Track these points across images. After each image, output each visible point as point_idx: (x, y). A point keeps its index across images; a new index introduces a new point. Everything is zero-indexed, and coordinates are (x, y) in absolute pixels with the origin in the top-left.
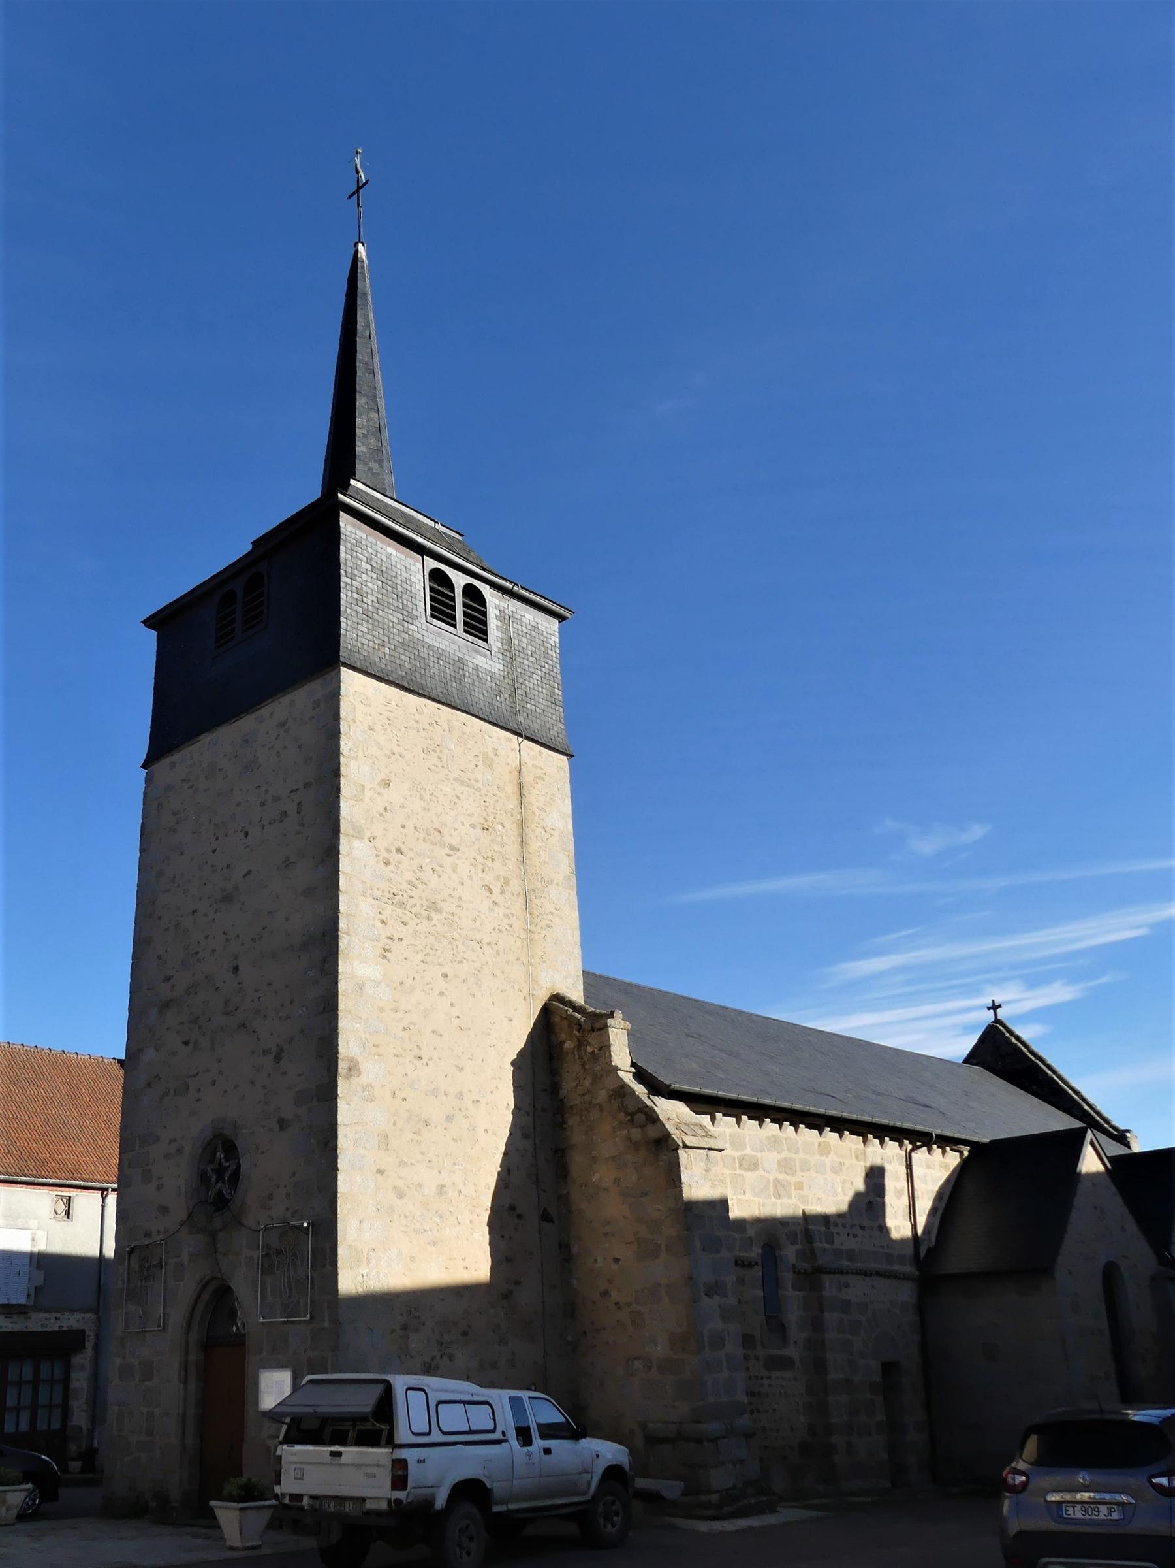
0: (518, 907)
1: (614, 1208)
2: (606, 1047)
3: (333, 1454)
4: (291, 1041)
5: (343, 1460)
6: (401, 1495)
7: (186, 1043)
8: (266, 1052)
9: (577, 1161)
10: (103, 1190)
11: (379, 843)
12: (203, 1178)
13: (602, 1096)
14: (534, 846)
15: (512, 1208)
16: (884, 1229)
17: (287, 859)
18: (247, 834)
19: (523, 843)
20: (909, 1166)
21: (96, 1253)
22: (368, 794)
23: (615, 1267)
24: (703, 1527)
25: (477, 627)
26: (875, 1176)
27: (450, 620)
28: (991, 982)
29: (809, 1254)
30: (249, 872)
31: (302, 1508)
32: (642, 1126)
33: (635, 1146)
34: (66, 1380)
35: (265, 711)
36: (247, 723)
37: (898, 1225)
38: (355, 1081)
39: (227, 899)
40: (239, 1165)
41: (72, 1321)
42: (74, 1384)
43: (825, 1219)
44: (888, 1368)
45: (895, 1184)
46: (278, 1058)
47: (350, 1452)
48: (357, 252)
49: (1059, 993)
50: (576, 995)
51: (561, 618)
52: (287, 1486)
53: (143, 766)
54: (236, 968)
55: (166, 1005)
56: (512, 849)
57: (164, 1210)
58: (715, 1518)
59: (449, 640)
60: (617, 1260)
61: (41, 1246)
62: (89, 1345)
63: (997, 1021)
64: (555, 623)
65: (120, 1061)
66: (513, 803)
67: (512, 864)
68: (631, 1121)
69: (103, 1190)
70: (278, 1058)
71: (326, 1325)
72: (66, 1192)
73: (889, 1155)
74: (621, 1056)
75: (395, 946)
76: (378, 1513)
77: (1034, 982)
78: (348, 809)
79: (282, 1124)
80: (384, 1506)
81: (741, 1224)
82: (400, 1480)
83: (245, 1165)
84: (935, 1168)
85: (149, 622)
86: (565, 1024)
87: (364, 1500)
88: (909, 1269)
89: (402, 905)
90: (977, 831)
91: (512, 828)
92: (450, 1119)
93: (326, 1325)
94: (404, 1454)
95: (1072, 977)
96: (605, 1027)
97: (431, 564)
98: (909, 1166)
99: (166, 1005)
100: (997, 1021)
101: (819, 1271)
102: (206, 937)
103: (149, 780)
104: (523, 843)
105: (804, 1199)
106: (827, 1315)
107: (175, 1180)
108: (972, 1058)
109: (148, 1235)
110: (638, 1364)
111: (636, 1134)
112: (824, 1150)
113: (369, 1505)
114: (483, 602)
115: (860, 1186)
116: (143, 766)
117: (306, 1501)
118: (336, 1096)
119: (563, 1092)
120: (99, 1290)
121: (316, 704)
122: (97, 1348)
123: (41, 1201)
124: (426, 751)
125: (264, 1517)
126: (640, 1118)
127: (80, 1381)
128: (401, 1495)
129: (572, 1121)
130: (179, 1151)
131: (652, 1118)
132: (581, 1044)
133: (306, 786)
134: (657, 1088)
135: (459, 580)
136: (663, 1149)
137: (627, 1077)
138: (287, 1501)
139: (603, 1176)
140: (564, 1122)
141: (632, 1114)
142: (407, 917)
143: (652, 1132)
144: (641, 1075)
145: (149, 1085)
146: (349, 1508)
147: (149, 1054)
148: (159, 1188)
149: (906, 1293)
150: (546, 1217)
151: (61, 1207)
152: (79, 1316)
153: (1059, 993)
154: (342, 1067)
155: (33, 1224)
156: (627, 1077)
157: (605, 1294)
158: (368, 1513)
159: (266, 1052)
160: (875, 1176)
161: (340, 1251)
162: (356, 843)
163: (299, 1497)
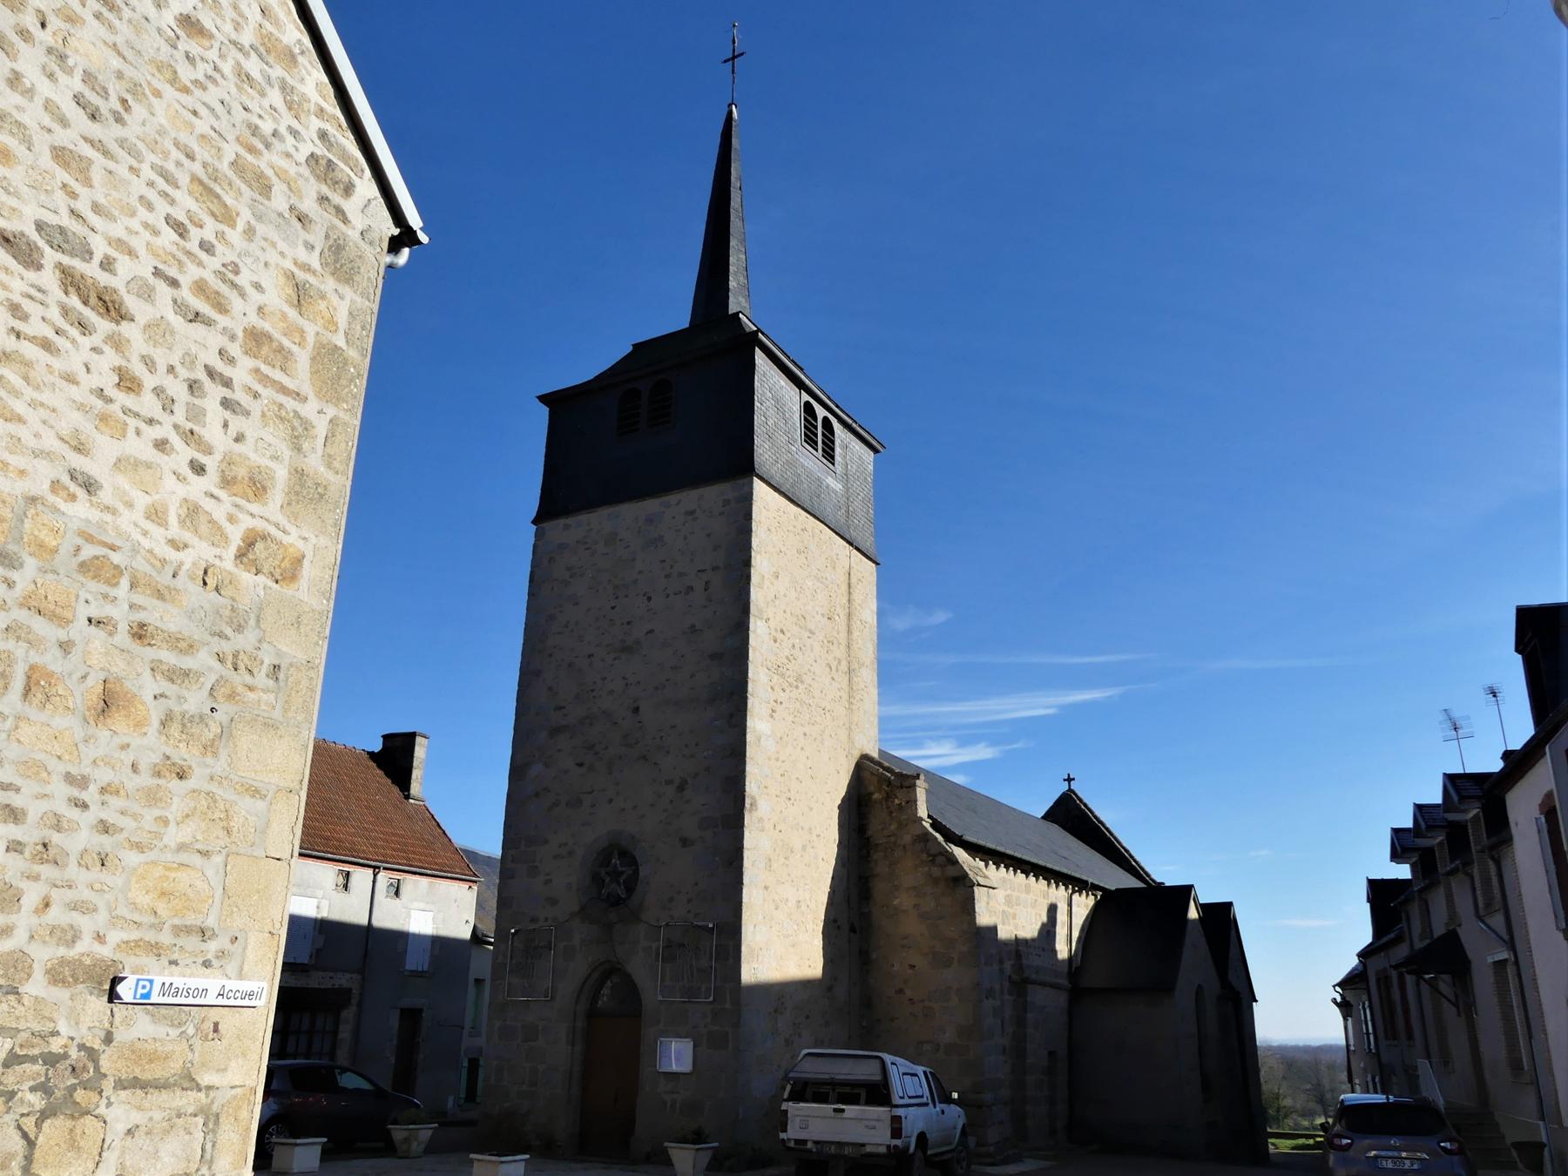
0: (845, 684)
1: (911, 926)
2: (913, 802)
3: (835, 1110)
4: (696, 775)
5: (845, 1115)
6: (898, 1142)
7: (580, 765)
8: (668, 782)
9: (879, 888)
10: (375, 868)
11: (772, 623)
12: (597, 880)
13: (907, 839)
14: (856, 634)
15: (835, 921)
16: (1054, 952)
17: (693, 626)
18: (649, 599)
19: (849, 632)
20: (1070, 905)
21: (365, 922)
22: (767, 583)
23: (910, 971)
24: (989, 1169)
25: (829, 454)
26: (1052, 909)
27: (813, 444)
28: (931, 738)
29: (1019, 967)
30: (651, 631)
31: (810, 1151)
32: (942, 866)
33: (936, 881)
34: (335, 1032)
35: (672, 498)
36: (651, 505)
37: (1062, 950)
38: (755, 814)
39: (626, 649)
40: (636, 872)
41: (342, 980)
42: (341, 1036)
43: (1025, 941)
44: (1051, 1054)
45: (1062, 917)
46: (681, 788)
47: (851, 1110)
48: (730, 112)
49: (982, 752)
50: (875, 755)
51: (876, 451)
52: (792, 1133)
53: (534, 522)
54: (636, 710)
55: (556, 731)
56: (843, 636)
57: (553, 901)
58: (993, 1164)
59: (810, 460)
60: (912, 967)
61: (324, 914)
62: (354, 1001)
63: (1070, 790)
64: (869, 456)
65: (372, 755)
66: (845, 600)
67: (843, 648)
68: (933, 861)
69: (375, 868)
70: (681, 788)
71: (728, 1006)
72: (346, 868)
73: (1059, 894)
74: (922, 812)
75: (778, 708)
76: (878, 1155)
77: (964, 742)
78: (757, 595)
79: (685, 842)
80: (883, 1150)
81: (1006, 943)
82: (896, 1132)
83: (643, 872)
84: (1084, 904)
85: (544, 399)
86: (875, 780)
87: (863, 1145)
88: (1064, 982)
89: (783, 675)
90: (940, 617)
91: (844, 618)
92: (804, 848)
93: (728, 1006)
94: (900, 1112)
95: (994, 741)
96: (914, 785)
97: (806, 397)
98: (1070, 905)
99: (556, 731)
100: (1070, 790)
101: (1026, 981)
102: (604, 679)
103: (539, 535)
104: (849, 632)
105: (1016, 927)
106: (1029, 1015)
107: (564, 879)
108: (1050, 816)
109: (533, 920)
110: (927, 1047)
111: (936, 872)
112: (1028, 890)
113: (868, 1149)
114: (832, 433)
115: (1045, 919)
116: (534, 522)
117: (810, 1145)
118: (742, 825)
119: (869, 833)
120: (366, 955)
121: (726, 502)
122: (360, 1004)
123: (326, 873)
124: (799, 552)
125: (705, 1158)
126: (940, 859)
127: (345, 1033)
128: (898, 1142)
129: (876, 856)
130: (570, 853)
131: (953, 861)
132: (889, 797)
133: (715, 569)
134: (951, 837)
135: (821, 412)
136: (962, 886)
137: (927, 825)
138: (792, 1144)
139: (904, 900)
140: (868, 855)
141: (934, 856)
142: (785, 685)
143: (951, 871)
144: (936, 825)
145: (537, 795)
146: (847, 1151)
147: (536, 770)
148: (548, 882)
149: (1062, 999)
150: (853, 930)
151: (341, 880)
152: (348, 976)
153: (982, 752)
154: (748, 802)
155: (320, 893)
156: (927, 825)
157: (901, 991)
158: (871, 1155)
159: (668, 782)
160: (1052, 909)
161: (743, 949)
162: (759, 623)
163: (804, 1142)
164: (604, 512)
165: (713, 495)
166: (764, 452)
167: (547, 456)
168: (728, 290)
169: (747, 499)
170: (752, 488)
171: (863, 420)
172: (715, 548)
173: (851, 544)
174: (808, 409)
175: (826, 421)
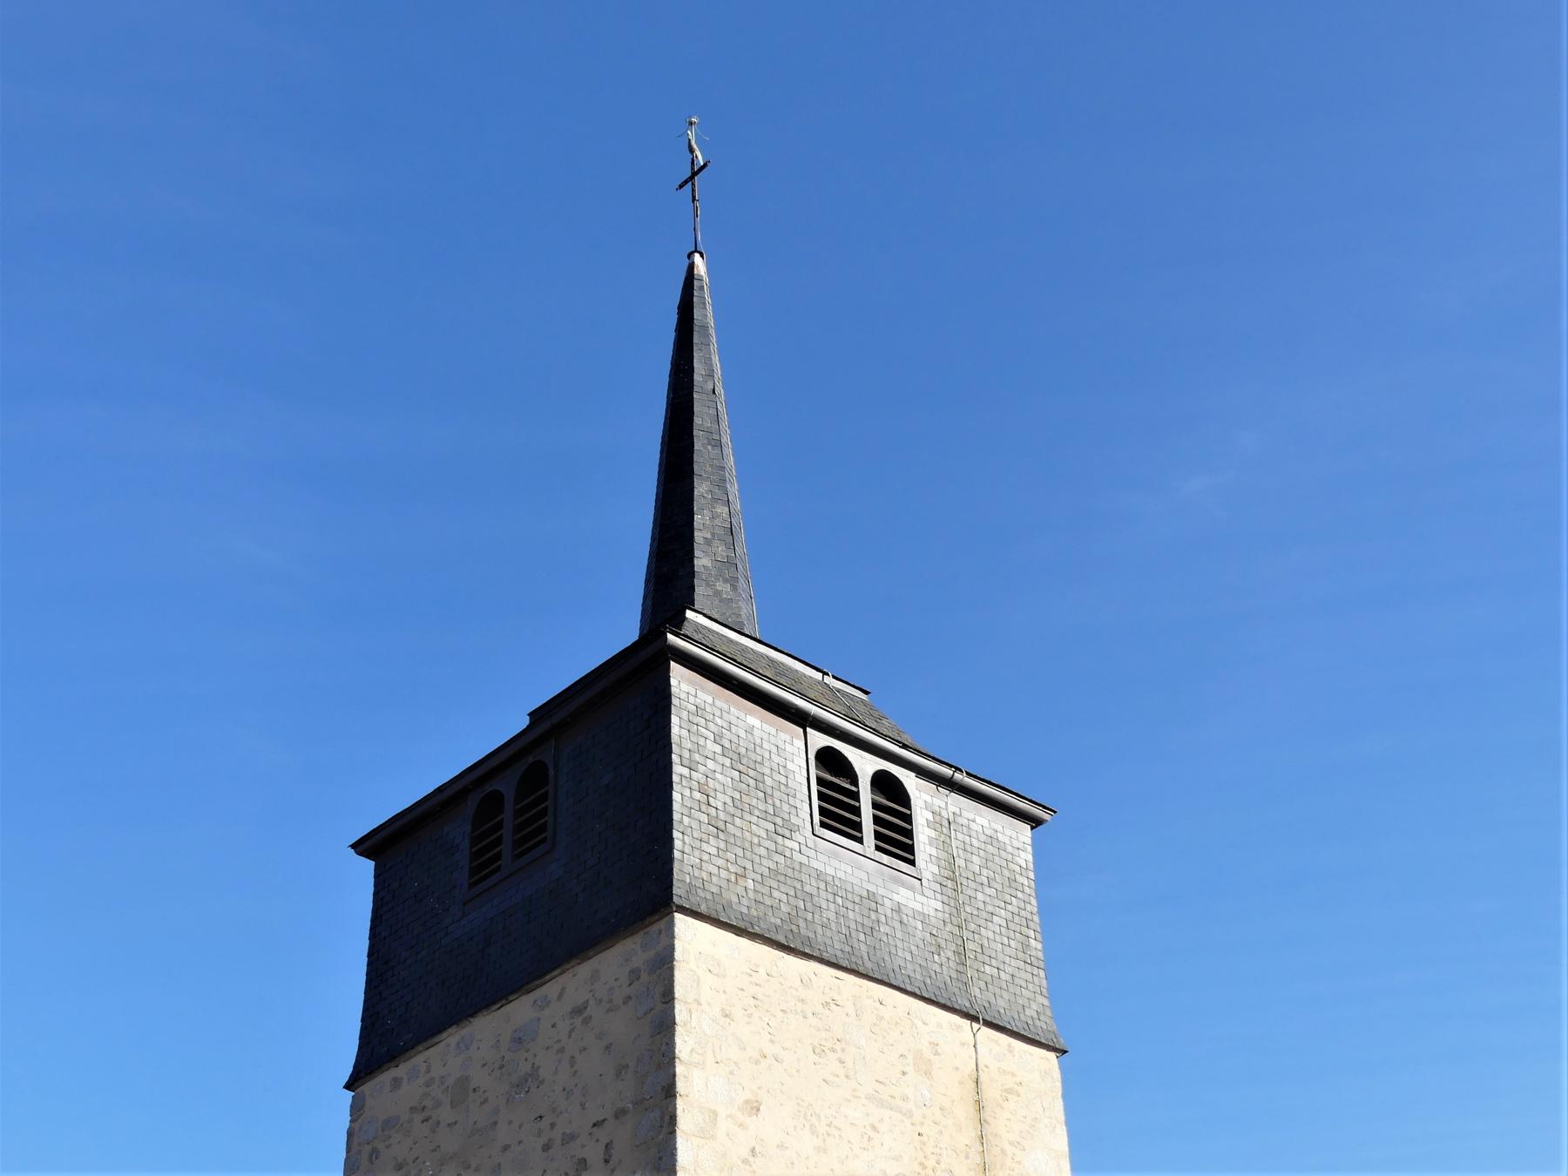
25: (897, 840)
36: (520, 1009)
48: (691, 267)
51: (1035, 822)
59: (853, 865)
66: (968, 1136)
85: (363, 847)
97: (819, 740)
103: (356, 1109)
116: (349, 1086)
121: (635, 975)
135: (865, 765)
164: (452, 1038)
165: (612, 964)
166: (695, 854)
167: (371, 954)
168: (692, 574)
169: (664, 962)
170: (671, 936)
171: (972, 761)
172: (620, 1071)
173: (974, 1018)
174: (827, 758)
175: (883, 782)
